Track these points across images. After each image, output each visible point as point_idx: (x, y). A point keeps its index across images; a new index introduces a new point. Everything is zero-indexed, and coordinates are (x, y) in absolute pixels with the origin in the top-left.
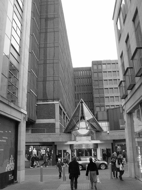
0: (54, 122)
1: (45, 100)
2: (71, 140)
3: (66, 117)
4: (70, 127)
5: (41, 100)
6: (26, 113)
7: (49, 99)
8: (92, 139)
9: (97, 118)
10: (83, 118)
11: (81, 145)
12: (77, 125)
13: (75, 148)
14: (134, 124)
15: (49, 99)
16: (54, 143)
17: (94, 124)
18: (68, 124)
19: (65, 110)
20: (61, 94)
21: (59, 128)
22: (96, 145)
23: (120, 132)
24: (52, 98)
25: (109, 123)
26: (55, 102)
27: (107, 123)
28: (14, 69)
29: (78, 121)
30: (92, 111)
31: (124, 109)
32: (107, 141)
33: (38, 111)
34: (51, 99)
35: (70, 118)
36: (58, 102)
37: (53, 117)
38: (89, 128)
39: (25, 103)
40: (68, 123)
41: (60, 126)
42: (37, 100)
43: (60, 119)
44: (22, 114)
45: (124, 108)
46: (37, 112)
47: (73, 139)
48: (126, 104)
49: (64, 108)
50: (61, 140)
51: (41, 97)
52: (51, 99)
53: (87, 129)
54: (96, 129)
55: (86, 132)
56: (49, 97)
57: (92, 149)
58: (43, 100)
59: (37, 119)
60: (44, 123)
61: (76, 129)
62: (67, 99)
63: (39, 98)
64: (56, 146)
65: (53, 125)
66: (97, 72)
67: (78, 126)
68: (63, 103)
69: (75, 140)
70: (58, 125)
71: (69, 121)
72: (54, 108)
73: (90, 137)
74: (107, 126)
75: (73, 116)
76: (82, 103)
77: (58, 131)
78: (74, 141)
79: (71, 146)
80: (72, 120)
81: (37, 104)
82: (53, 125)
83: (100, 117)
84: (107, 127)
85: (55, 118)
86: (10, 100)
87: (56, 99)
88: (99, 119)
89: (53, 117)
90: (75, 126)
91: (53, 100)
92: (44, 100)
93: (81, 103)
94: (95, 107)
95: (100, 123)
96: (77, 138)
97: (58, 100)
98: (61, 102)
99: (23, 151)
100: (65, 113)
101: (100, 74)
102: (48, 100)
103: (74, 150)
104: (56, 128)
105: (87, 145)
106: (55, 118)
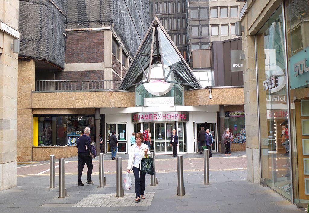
0: (102, 69)
1: (83, 23)
2: (134, 105)
3: (123, 52)
4: (134, 77)
5: (75, 23)
6: (18, 35)
7: (92, 22)
8: (178, 103)
9: (189, 61)
10: (157, 59)
11: (152, 115)
12: (146, 74)
13: (140, 121)
14: (266, 62)
15: (92, 22)
16: (98, 109)
17: (183, 75)
18: (127, 69)
19: (127, 46)
20: (117, 10)
21: (112, 79)
22: (185, 116)
23: (234, 89)
24: (98, 19)
25: (213, 73)
26: (103, 27)
27: (209, 73)
28: (124, 56)
29: (148, 66)
30: (185, 52)
31: (244, 27)
32: (207, 108)
33: (68, 45)
34: (95, 20)
35: (133, 56)
36: (109, 28)
37: (100, 59)
38: (170, 79)
39: (15, 11)
40: (128, 66)
41: (114, 76)
42: (66, 23)
43: (115, 63)
44: (6, 37)
45: (242, 25)
46: (65, 50)
47: (139, 101)
48: (249, 15)
49: (124, 42)
50: (112, 105)
51: (73, 16)
52: (95, 22)
53: (166, 81)
54: (186, 82)
55: (165, 87)
56: (90, 17)
57: (176, 122)
58: (78, 23)
59: (66, 62)
60: (81, 70)
61: (144, 81)
62: (132, 25)
63: (69, 19)
64: (103, 117)
65: (100, 75)
66: (197, 8)
67: (147, 75)
68: (121, 32)
69: (142, 105)
70: (109, 74)
71: (130, 62)
72: (102, 39)
73: (172, 99)
74: (210, 79)
75: (137, 55)
76: (156, 26)
77: (109, 85)
78: (140, 106)
79: (134, 116)
80: (135, 62)
81: (67, 32)
82: (100, 75)
83: (196, 62)
84: (210, 82)
85: (102, 60)
86: (97, 78)
87: (105, 21)
88: (196, 64)
89: (100, 59)
90: (141, 76)
91: (100, 22)
92: (80, 23)
93: (154, 25)
94: (190, 45)
95: (196, 74)
96: (148, 100)
97: (110, 22)
98: (115, 28)
99: (11, 122)
100: (128, 53)
101: (203, 12)
102: (88, 22)
103: (140, 124)
104: (105, 79)
105: (166, 115)
106: (102, 60)
